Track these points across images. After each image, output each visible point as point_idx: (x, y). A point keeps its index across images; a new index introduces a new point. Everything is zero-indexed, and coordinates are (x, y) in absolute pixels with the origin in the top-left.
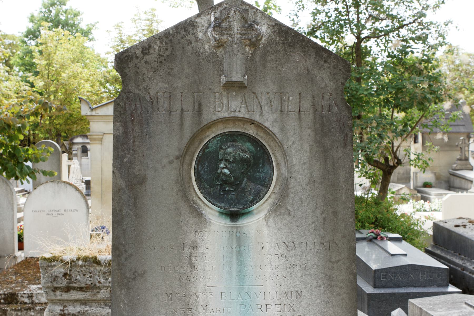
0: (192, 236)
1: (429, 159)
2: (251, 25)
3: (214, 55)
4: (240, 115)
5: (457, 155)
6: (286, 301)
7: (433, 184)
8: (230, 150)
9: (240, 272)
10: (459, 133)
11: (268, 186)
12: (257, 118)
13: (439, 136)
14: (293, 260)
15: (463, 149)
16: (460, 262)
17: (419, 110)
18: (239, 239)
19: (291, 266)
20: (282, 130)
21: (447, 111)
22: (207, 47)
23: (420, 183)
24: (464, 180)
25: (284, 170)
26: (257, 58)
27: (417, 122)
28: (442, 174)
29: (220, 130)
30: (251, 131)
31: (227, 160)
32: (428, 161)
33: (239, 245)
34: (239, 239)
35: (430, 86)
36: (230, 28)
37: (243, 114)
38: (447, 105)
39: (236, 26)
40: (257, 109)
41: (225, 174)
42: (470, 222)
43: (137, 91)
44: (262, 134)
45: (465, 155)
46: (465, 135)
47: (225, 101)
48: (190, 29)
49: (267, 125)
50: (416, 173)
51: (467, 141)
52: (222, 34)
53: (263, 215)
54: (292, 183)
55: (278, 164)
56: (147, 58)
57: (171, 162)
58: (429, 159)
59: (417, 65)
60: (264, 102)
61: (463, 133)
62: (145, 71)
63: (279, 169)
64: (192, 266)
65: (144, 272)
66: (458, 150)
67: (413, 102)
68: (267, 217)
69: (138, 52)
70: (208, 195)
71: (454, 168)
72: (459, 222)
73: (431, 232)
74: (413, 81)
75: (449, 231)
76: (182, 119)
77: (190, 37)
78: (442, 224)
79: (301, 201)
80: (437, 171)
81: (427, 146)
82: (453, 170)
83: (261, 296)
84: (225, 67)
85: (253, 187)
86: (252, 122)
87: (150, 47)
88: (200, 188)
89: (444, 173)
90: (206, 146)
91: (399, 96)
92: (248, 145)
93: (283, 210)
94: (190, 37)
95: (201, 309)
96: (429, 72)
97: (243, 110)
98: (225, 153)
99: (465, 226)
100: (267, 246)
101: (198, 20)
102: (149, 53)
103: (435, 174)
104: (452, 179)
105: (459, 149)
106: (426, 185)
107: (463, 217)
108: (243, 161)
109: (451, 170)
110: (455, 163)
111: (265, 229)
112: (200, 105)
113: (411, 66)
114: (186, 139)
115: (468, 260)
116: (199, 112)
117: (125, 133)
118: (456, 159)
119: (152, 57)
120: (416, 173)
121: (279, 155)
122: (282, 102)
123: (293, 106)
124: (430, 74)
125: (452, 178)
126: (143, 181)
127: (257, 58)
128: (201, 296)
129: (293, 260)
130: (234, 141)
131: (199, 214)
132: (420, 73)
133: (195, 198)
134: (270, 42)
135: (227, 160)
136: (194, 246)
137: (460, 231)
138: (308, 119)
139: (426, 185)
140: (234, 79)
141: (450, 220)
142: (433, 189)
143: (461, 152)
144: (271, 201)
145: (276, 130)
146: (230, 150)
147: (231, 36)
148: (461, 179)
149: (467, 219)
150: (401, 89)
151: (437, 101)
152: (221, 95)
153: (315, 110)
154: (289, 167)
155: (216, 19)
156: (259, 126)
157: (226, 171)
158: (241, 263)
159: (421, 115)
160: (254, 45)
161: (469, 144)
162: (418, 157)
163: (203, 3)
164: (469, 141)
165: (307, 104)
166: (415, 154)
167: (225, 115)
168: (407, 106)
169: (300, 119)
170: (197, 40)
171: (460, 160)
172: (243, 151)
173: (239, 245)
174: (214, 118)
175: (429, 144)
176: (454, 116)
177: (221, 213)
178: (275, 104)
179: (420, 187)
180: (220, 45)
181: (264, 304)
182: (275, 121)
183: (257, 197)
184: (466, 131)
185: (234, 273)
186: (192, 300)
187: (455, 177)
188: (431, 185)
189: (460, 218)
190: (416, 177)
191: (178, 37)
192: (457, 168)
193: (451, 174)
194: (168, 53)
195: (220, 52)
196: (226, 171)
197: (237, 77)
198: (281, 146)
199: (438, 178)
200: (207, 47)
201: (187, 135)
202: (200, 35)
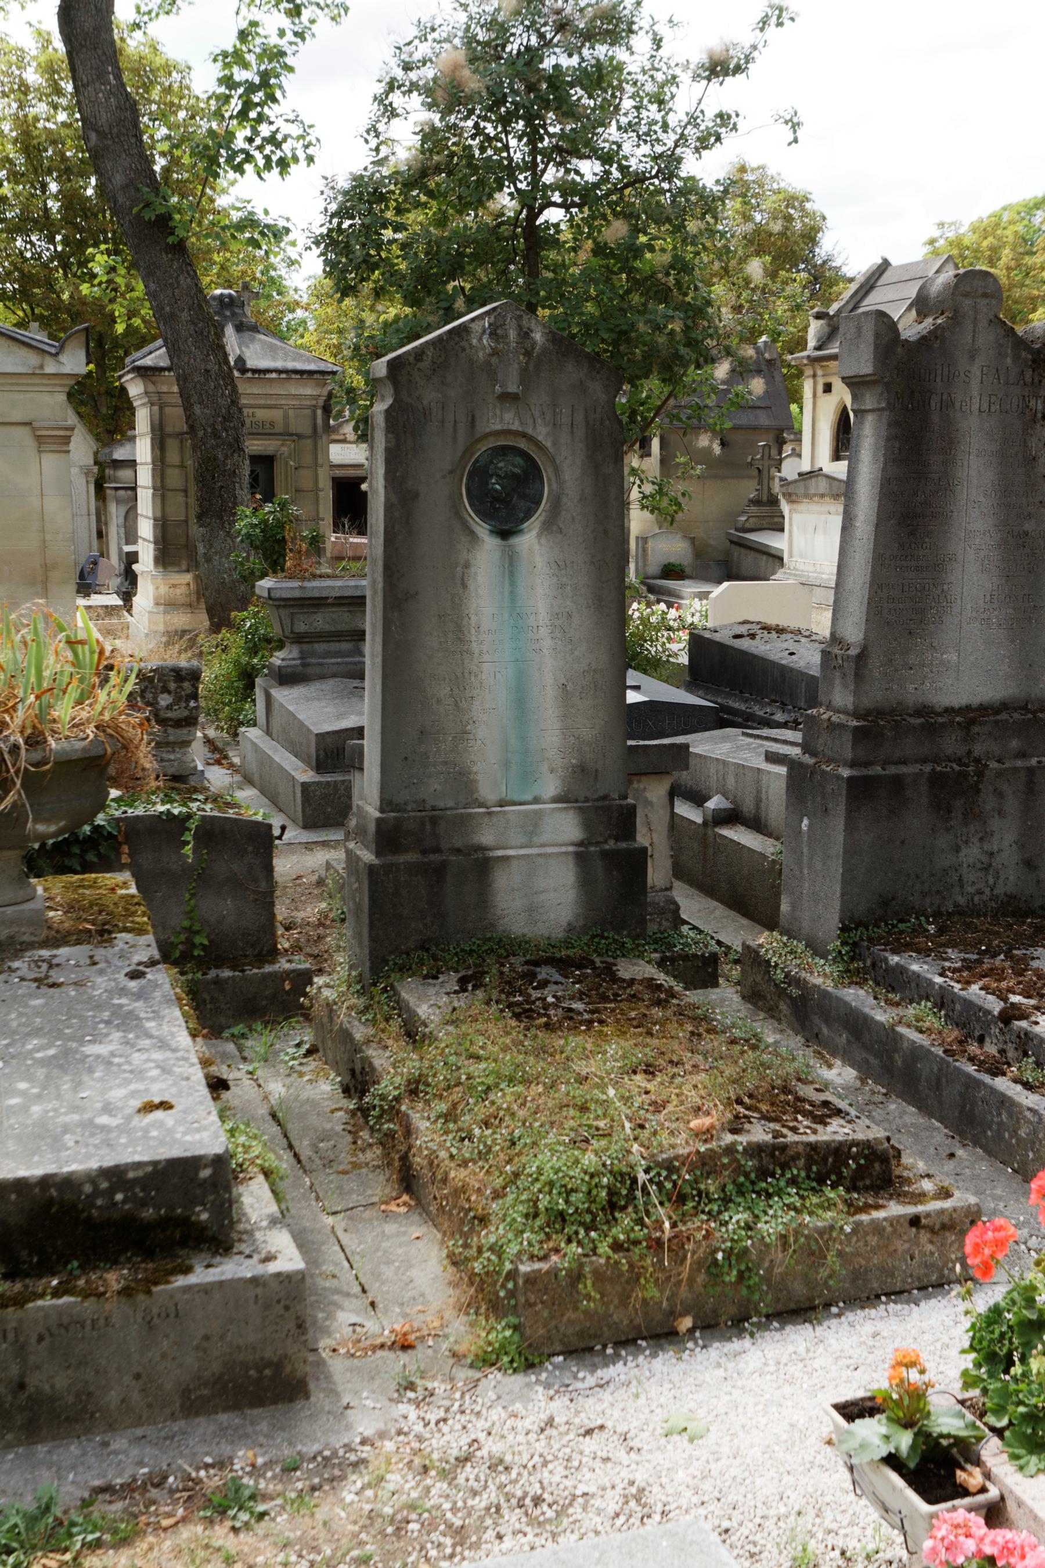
0: (464, 555)
1: (683, 494)
2: (526, 333)
3: (488, 363)
4: (514, 428)
5: (749, 489)
6: (557, 622)
7: (688, 570)
8: (501, 465)
9: (512, 592)
10: (755, 429)
11: (538, 503)
12: (530, 431)
13: (704, 441)
14: (564, 580)
15: (765, 473)
16: (743, 707)
17: (664, 381)
18: (511, 558)
19: (563, 586)
20: (554, 444)
21: (723, 383)
22: (481, 354)
23: (653, 568)
24: (764, 557)
25: (555, 486)
26: (531, 368)
27: (660, 408)
28: (712, 542)
29: (492, 443)
30: (522, 444)
31: (498, 476)
32: (680, 499)
33: (511, 564)
34: (511, 558)
35: (687, 329)
36: (506, 336)
37: (516, 426)
38: (722, 370)
39: (512, 334)
40: (530, 422)
41: (496, 490)
42: (763, 628)
43: (409, 400)
44: (533, 448)
45: (769, 489)
46: (771, 436)
47: (498, 412)
48: (464, 334)
49: (540, 438)
50: (645, 540)
51: (774, 452)
52: (497, 342)
53: (534, 533)
54: (564, 499)
55: (549, 480)
56: (420, 365)
57: (444, 477)
58: (683, 494)
59: (660, 276)
60: (537, 414)
61: (767, 429)
62: (418, 379)
63: (550, 485)
64: (465, 586)
65: (417, 593)
66: (750, 477)
67: (651, 364)
68: (539, 536)
69: (411, 359)
70: (478, 512)
71: (740, 525)
72: (743, 629)
73: (684, 659)
74: (652, 317)
75: (721, 646)
76: (455, 431)
77: (464, 344)
78: (707, 635)
79: (573, 518)
80: (699, 533)
81: (679, 464)
82: (737, 530)
83: (532, 618)
84: (500, 377)
85: (523, 504)
86: (524, 435)
87: (423, 353)
88: (471, 505)
89: (716, 540)
90: (477, 461)
91: (622, 348)
92: (519, 460)
93: (555, 528)
94: (464, 344)
95: (473, 631)
96: (686, 294)
97: (517, 423)
98: (496, 468)
99: (753, 636)
100: (539, 565)
101: (472, 325)
102: (422, 360)
103: (693, 540)
104: (736, 554)
105: (756, 473)
106: (672, 572)
107: (751, 619)
108: (514, 476)
109: (732, 531)
110: (743, 512)
111: (537, 547)
112: (473, 417)
113: (646, 279)
114: (459, 454)
115: (756, 701)
116: (472, 423)
117: (398, 446)
118: (746, 502)
119: (425, 364)
120: (645, 540)
121: (550, 470)
122: (554, 414)
123: (565, 420)
124: (688, 299)
125: (736, 551)
126: (416, 496)
127: (531, 368)
128: (473, 617)
129: (564, 580)
130: (505, 455)
131: (472, 533)
132: (664, 295)
133: (466, 516)
134: (544, 351)
135: (498, 476)
136: (467, 566)
137: (745, 644)
138: (580, 432)
139: (672, 572)
140: (510, 390)
141: (725, 627)
142: (687, 582)
143: (760, 483)
144: (541, 519)
145: (548, 444)
146: (501, 465)
147: (508, 344)
148: (758, 555)
149: (758, 623)
150: (625, 333)
151: (702, 359)
152: (495, 407)
153: (587, 423)
154: (560, 482)
155: (490, 325)
156: (531, 439)
157: (498, 487)
158: (513, 584)
159: (666, 394)
160: (528, 354)
161: (781, 461)
162: (660, 489)
163: (85, 46)
164: (780, 453)
165: (579, 417)
166: (653, 483)
167: (498, 427)
168: (638, 373)
169: (572, 433)
170: (471, 346)
171: (756, 502)
172: (515, 466)
173: (511, 564)
174: (488, 430)
175: (682, 460)
176: (737, 395)
177: (492, 532)
178: (548, 417)
179: (655, 578)
180: (495, 353)
181: (535, 624)
182: (548, 434)
183: (528, 515)
184: (773, 423)
185: (507, 594)
186: (465, 622)
187: (743, 550)
188: (683, 571)
189: (745, 622)
190: (644, 550)
191: (452, 343)
192: (747, 525)
193: (732, 542)
194: (441, 360)
195: (494, 360)
196: (498, 487)
197: (512, 388)
198: (553, 461)
199: (700, 551)
200: (481, 354)
201: (461, 446)
202: (474, 342)
